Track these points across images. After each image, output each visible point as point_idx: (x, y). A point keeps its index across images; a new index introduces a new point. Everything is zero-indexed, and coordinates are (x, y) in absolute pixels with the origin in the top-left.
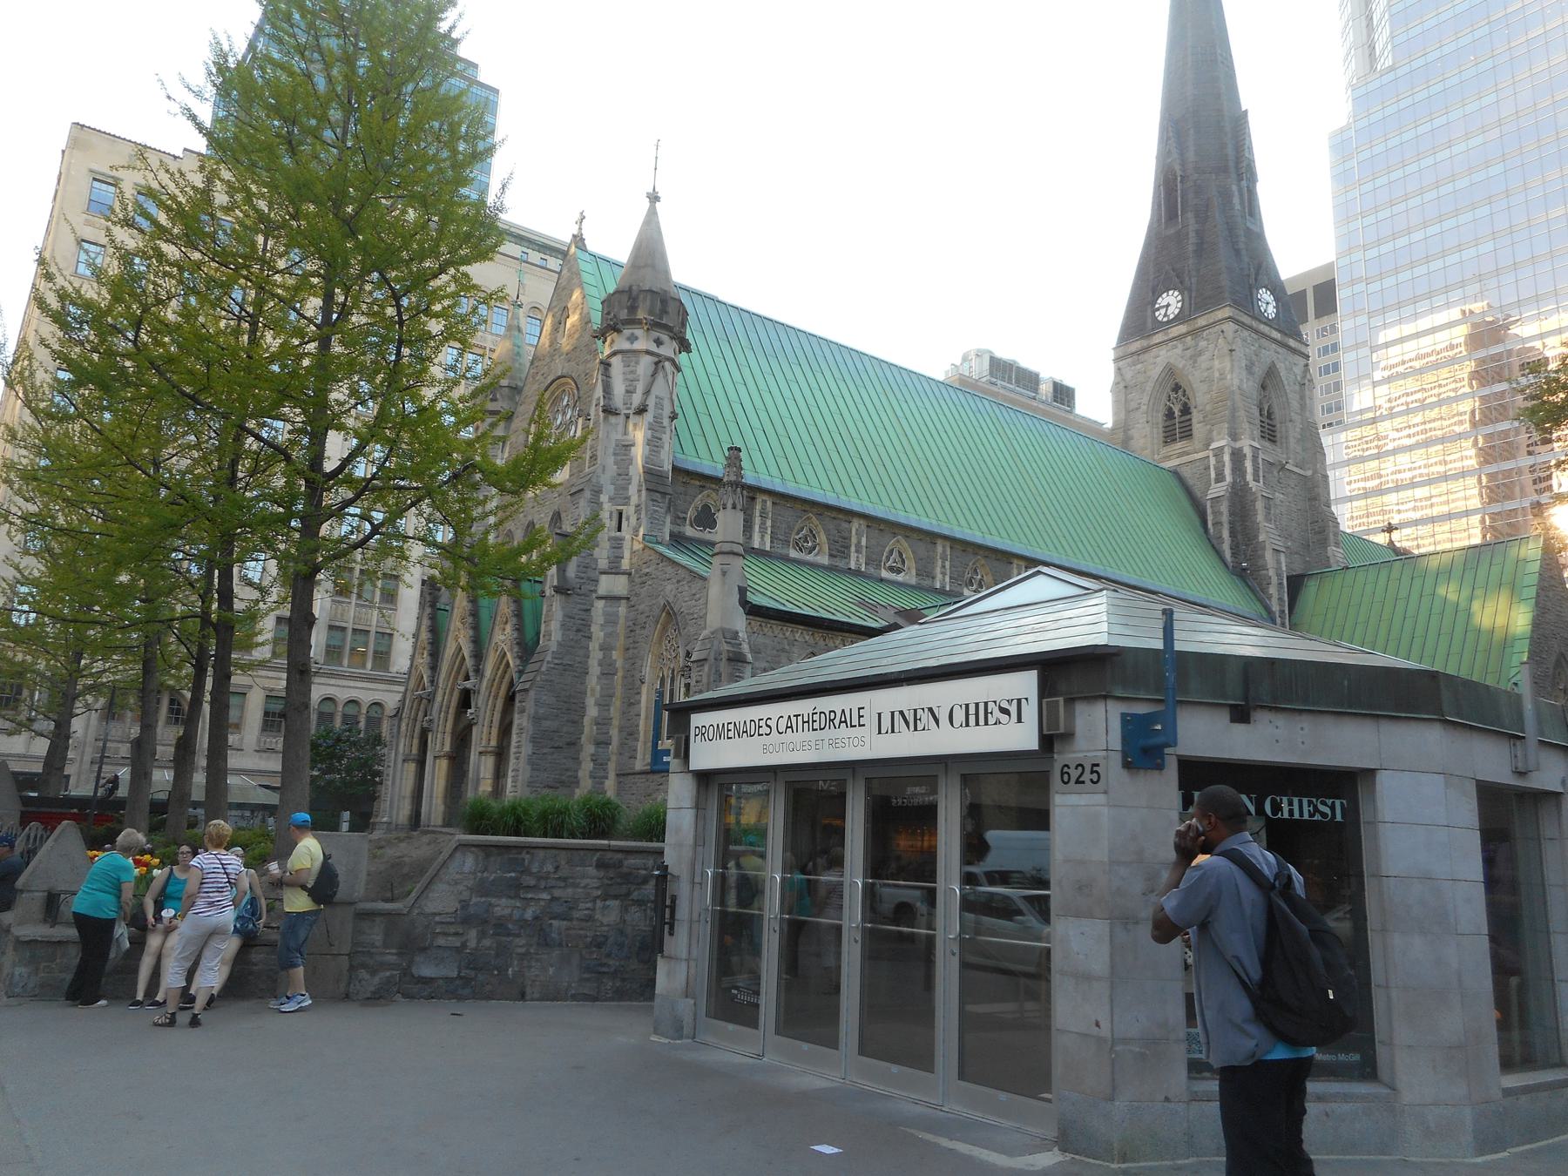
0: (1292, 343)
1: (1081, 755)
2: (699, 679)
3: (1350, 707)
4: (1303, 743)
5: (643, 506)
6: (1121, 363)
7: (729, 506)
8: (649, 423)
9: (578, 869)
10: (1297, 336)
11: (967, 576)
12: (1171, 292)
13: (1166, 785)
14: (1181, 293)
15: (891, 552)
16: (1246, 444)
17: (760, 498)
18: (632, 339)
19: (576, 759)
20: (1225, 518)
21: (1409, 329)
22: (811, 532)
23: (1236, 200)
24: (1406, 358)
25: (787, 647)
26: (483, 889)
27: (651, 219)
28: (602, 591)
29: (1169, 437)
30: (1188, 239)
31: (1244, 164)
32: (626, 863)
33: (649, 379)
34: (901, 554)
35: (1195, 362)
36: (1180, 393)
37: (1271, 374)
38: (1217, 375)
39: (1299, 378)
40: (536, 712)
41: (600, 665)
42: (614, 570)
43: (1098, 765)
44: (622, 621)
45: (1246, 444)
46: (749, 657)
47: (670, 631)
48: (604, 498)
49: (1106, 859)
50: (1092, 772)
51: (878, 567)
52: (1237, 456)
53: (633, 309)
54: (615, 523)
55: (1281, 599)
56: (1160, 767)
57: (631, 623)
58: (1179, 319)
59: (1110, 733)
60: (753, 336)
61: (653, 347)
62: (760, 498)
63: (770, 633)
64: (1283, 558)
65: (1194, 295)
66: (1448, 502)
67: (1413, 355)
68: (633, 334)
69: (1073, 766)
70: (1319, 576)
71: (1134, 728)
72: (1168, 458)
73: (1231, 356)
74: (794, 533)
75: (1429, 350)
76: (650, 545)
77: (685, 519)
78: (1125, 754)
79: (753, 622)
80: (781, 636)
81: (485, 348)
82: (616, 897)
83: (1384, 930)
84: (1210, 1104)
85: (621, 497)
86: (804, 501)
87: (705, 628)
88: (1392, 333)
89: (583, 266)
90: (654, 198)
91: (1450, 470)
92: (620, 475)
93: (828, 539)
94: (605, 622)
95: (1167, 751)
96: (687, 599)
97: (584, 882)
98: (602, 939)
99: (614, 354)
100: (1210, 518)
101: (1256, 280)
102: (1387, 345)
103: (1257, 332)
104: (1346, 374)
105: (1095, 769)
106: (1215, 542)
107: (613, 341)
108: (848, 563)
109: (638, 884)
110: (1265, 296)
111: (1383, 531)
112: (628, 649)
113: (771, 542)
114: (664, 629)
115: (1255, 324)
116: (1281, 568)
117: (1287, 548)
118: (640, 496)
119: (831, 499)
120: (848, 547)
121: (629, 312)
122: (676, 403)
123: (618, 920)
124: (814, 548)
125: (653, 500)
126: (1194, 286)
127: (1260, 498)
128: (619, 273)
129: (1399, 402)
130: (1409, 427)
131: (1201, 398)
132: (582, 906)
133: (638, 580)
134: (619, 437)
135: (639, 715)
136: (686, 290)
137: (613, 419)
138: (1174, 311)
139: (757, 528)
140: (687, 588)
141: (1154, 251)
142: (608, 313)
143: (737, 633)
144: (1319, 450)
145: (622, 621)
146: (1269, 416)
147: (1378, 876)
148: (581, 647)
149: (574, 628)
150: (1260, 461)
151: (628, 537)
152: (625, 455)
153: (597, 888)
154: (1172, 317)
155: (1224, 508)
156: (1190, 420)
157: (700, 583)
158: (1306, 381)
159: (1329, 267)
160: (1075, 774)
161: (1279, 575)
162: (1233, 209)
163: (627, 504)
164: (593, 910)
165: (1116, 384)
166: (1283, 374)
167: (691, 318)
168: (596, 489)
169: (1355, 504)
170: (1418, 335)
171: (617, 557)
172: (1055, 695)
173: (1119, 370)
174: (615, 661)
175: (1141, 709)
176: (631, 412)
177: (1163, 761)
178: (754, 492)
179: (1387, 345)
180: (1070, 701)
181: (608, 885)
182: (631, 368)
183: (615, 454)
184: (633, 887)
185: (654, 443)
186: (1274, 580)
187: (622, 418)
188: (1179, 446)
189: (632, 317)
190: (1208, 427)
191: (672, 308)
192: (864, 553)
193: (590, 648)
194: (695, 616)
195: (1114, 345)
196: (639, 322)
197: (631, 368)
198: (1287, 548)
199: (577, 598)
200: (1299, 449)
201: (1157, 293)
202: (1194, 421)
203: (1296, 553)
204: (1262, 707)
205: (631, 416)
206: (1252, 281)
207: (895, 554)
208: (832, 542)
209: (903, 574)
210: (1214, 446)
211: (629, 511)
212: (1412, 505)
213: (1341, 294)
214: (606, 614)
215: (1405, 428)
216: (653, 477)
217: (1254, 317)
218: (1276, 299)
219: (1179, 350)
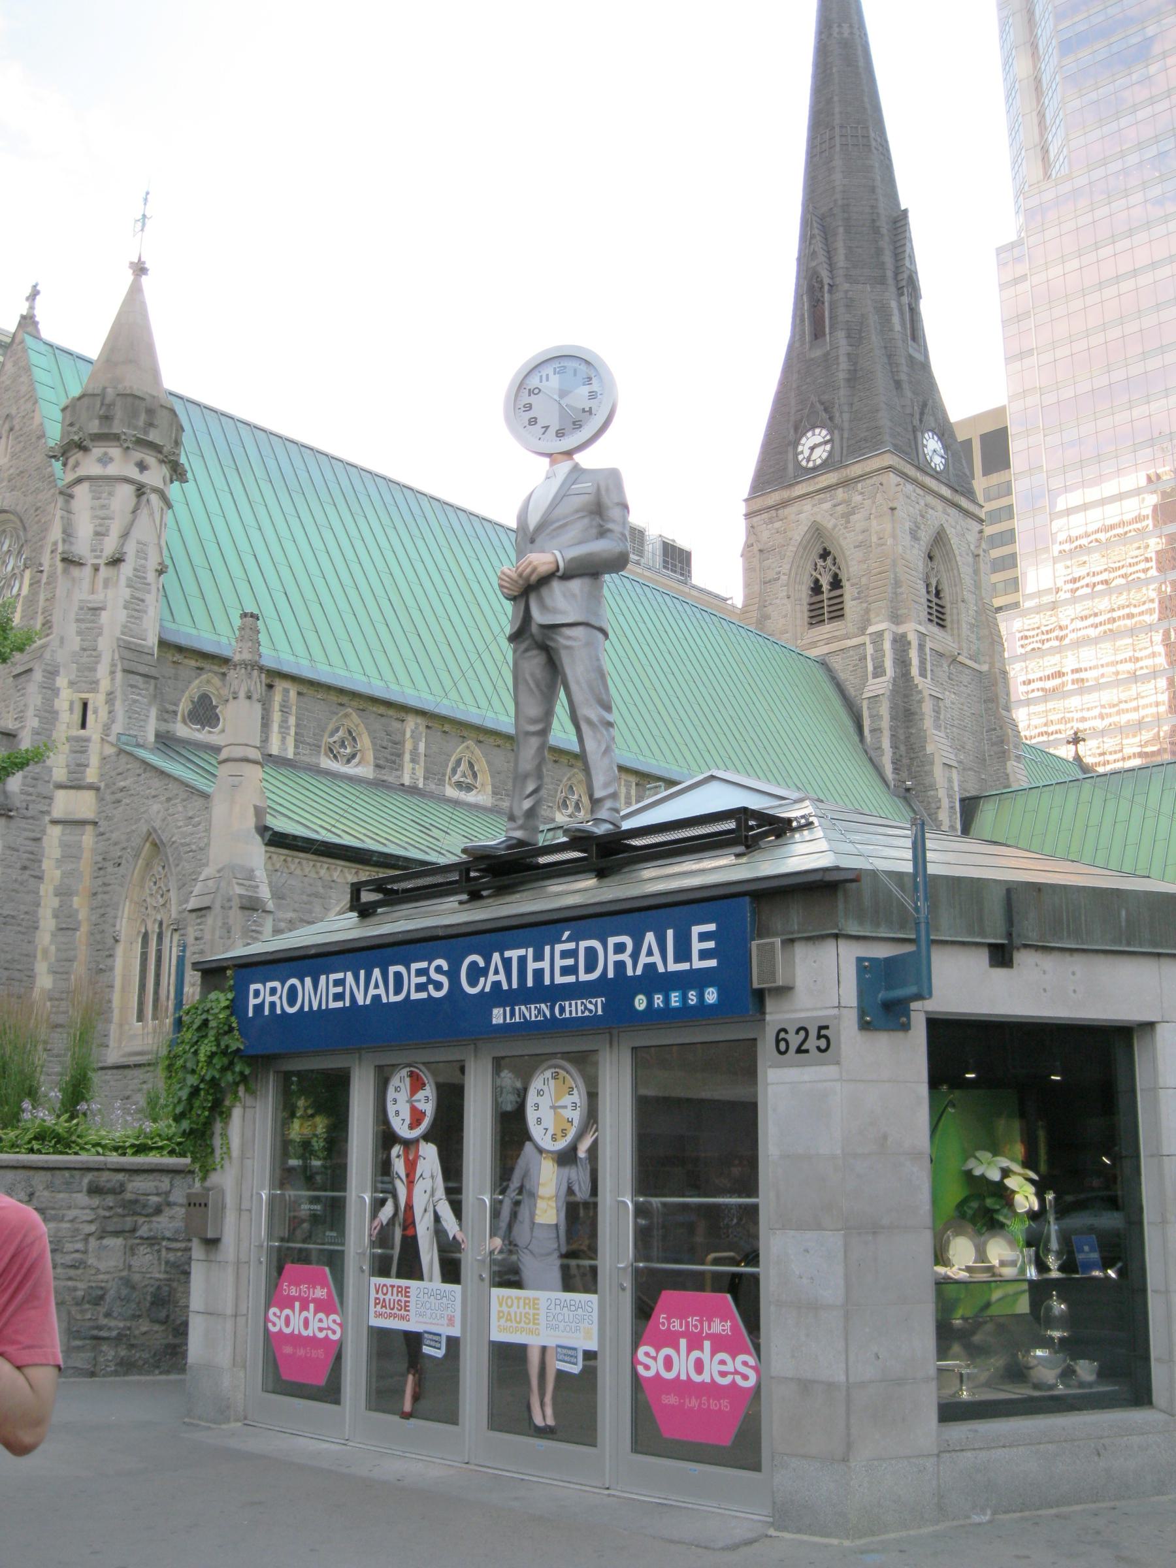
0: (964, 503)
1: (803, 1015)
2: (198, 934)
3: (1129, 944)
4: (1075, 991)
5: (118, 694)
6: (755, 519)
7: (242, 694)
8: (129, 579)
9: (61, 1195)
10: (970, 494)
11: (560, 796)
12: (817, 431)
14: (831, 432)
16: (911, 629)
17: (280, 685)
18: (105, 460)
20: (885, 724)
21: (1093, 494)
22: (350, 733)
23: (896, 319)
24: (1090, 530)
25: (321, 890)
27: (134, 300)
28: (58, 812)
29: (816, 617)
30: (838, 364)
31: (905, 276)
32: (130, 1186)
33: (130, 517)
34: (471, 765)
35: (848, 522)
36: (829, 560)
37: (940, 538)
38: (874, 539)
39: (972, 547)
41: (56, 916)
42: (75, 785)
43: (827, 1027)
44: (87, 855)
45: (911, 629)
46: (270, 905)
47: (157, 869)
48: (61, 682)
49: (839, 1152)
50: (819, 1037)
51: (441, 782)
52: (901, 643)
53: (107, 418)
56: (906, 1027)
57: (99, 858)
58: (827, 465)
59: (841, 985)
60: (271, 464)
61: (134, 473)
63: (298, 872)
64: (955, 775)
65: (846, 435)
66: (1136, 709)
67: (1098, 525)
68: (106, 454)
69: (792, 1031)
70: (998, 797)
72: (814, 644)
73: (893, 515)
74: (326, 735)
75: (1116, 520)
76: (128, 748)
77: (175, 713)
78: (862, 1012)
79: (275, 857)
80: (315, 876)
82: (117, 1233)
83: (1164, 1222)
84: (964, 1453)
85: (86, 678)
86: (341, 691)
87: (206, 865)
88: (1074, 499)
89: (35, 358)
90: (140, 269)
91: (1142, 668)
92: (84, 650)
93: (374, 744)
94: (63, 857)
95: (914, 1005)
96: (180, 824)
97: (71, 1214)
98: (100, 1293)
99: (79, 481)
100: (867, 723)
101: (921, 421)
102: (1069, 512)
103: (923, 486)
104: (1021, 546)
105: (823, 1032)
106: (873, 754)
107: (77, 465)
109: (147, 1216)
110: (932, 444)
111: (1069, 742)
112: (95, 894)
113: (296, 747)
114: (148, 865)
115: (919, 476)
116: (952, 788)
117: (960, 762)
118: (113, 679)
119: (377, 688)
120: (400, 755)
121: (101, 424)
122: (165, 552)
123: (121, 1267)
124: (354, 756)
125: (132, 686)
126: (846, 425)
127: (927, 698)
128: (86, 370)
129: (1083, 582)
130: (1096, 615)
131: (853, 568)
132: (69, 1247)
133: (109, 798)
134: (85, 596)
135: (112, 987)
136: (181, 398)
137: (75, 572)
138: (820, 454)
140: (180, 809)
141: (795, 376)
142: (71, 425)
143: (253, 871)
144: (994, 640)
145: (87, 855)
146: (938, 594)
147: (1158, 1155)
148: (28, 892)
149: (18, 865)
150: (928, 651)
152: (93, 621)
153: (91, 1222)
154: (819, 462)
155: (884, 710)
156: (841, 596)
157: (199, 802)
158: (982, 553)
159: (1000, 412)
160: (795, 1040)
161: (950, 796)
162: (891, 330)
163: (94, 690)
164: (85, 1252)
165: (748, 546)
166: (954, 541)
167: (187, 438)
168: (49, 668)
169: (1033, 709)
170: (1103, 502)
171: (79, 765)
172: (768, 935)
173: (752, 530)
174: (77, 911)
175: (882, 952)
176: (101, 561)
177: (909, 1018)
178: (275, 675)
179: (1069, 512)
180: (789, 942)
181: (105, 1217)
182: (102, 502)
184: (141, 1220)
185: (135, 606)
186: (945, 803)
187: (87, 571)
188: (827, 629)
189: (106, 431)
190: (865, 605)
191: (162, 419)
192: (422, 764)
193: (42, 893)
194: (194, 847)
195: (746, 496)
196: (116, 438)
197: (102, 502)
198: (960, 762)
199: (23, 824)
200: (973, 637)
201: (800, 430)
202: (847, 597)
203: (970, 769)
204: (1026, 946)
205: (102, 568)
206: (916, 422)
207: (464, 766)
208: (379, 749)
209: (474, 792)
210: (871, 629)
211: (97, 701)
212: (1096, 712)
213: (1016, 446)
214: (64, 845)
215: (1090, 616)
216: (130, 651)
217: (918, 468)
218: (946, 447)
219: (827, 506)
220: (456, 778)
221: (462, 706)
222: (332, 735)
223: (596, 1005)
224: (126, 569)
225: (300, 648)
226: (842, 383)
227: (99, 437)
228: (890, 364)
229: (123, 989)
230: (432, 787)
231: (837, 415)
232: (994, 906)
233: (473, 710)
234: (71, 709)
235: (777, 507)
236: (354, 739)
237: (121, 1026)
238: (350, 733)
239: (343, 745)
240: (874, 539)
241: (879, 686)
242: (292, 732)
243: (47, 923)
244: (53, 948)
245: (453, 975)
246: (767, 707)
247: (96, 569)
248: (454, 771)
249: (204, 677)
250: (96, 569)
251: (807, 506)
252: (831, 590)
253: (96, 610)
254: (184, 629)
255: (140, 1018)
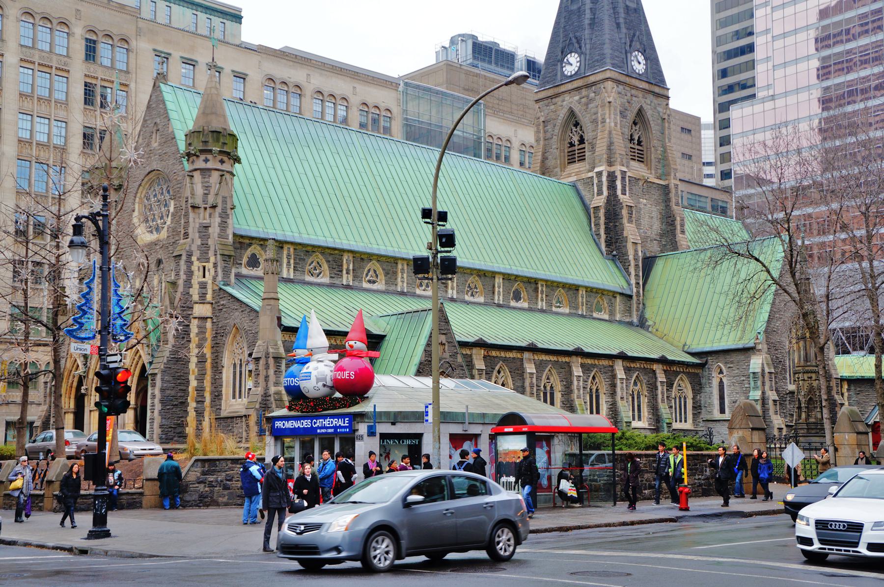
5: (219, 264)
8: (220, 214)
12: (573, 54)
13: (376, 440)
14: (580, 56)
15: (369, 271)
18: (206, 161)
19: (186, 412)
22: (318, 263)
26: (203, 473)
34: (375, 271)
36: (579, 127)
37: (640, 113)
38: (600, 119)
40: (162, 386)
47: (238, 338)
48: (194, 258)
51: (361, 281)
52: (612, 177)
54: (201, 273)
55: (637, 275)
61: (219, 166)
62: (286, 247)
68: (206, 158)
71: (370, 428)
77: (241, 264)
81: (51, 67)
99: (196, 170)
108: (342, 281)
115: (628, 80)
120: (341, 271)
124: (320, 273)
126: (588, 52)
127: (625, 207)
134: (201, 221)
137: (196, 210)
139: (285, 265)
151: (210, 282)
155: (602, 213)
161: (636, 259)
163: (208, 262)
183: (199, 232)
187: (202, 210)
188: (576, 167)
196: (210, 151)
197: (206, 180)
201: (564, 53)
203: (655, 240)
205: (208, 209)
206: (628, 48)
207: (371, 273)
211: (209, 266)
214: (199, 327)
218: (646, 59)
219: (577, 98)
220: (368, 278)
221: (370, 246)
222: (310, 265)
223: (332, 430)
224: (218, 210)
225: (294, 228)
226: (587, 27)
227: (202, 151)
228: (614, 13)
229: (226, 386)
230: (356, 284)
231: (583, 46)
232: (392, 416)
233: (375, 246)
234: (199, 270)
235: (551, 97)
236: (320, 266)
237: (226, 401)
238: (318, 263)
239: (315, 269)
240: (600, 119)
241: (600, 201)
242: (292, 267)
243: (194, 360)
244: (196, 370)
245: (311, 423)
246: (534, 219)
247: (205, 208)
248: (367, 275)
249: (253, 247)
250: (205, 208)
251: (567, 97)
252: (579, 145)
253: (207, 227)
254: (243, 227)
255: (234, 397)
